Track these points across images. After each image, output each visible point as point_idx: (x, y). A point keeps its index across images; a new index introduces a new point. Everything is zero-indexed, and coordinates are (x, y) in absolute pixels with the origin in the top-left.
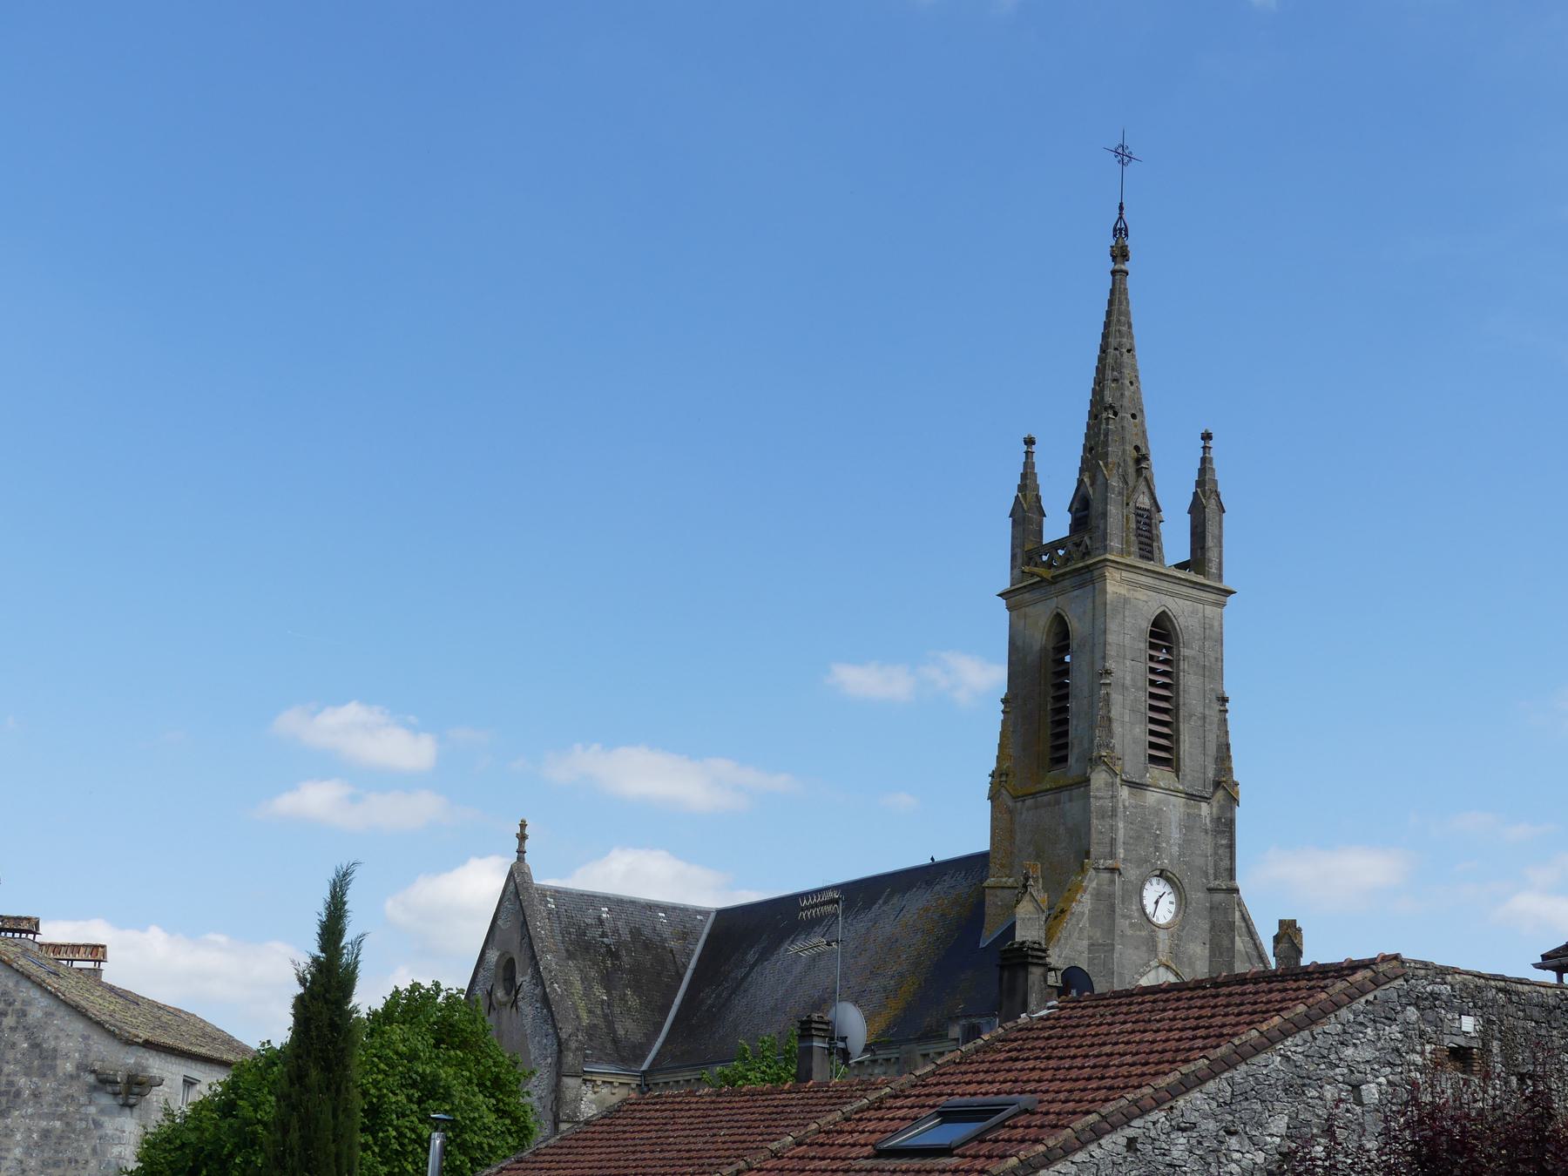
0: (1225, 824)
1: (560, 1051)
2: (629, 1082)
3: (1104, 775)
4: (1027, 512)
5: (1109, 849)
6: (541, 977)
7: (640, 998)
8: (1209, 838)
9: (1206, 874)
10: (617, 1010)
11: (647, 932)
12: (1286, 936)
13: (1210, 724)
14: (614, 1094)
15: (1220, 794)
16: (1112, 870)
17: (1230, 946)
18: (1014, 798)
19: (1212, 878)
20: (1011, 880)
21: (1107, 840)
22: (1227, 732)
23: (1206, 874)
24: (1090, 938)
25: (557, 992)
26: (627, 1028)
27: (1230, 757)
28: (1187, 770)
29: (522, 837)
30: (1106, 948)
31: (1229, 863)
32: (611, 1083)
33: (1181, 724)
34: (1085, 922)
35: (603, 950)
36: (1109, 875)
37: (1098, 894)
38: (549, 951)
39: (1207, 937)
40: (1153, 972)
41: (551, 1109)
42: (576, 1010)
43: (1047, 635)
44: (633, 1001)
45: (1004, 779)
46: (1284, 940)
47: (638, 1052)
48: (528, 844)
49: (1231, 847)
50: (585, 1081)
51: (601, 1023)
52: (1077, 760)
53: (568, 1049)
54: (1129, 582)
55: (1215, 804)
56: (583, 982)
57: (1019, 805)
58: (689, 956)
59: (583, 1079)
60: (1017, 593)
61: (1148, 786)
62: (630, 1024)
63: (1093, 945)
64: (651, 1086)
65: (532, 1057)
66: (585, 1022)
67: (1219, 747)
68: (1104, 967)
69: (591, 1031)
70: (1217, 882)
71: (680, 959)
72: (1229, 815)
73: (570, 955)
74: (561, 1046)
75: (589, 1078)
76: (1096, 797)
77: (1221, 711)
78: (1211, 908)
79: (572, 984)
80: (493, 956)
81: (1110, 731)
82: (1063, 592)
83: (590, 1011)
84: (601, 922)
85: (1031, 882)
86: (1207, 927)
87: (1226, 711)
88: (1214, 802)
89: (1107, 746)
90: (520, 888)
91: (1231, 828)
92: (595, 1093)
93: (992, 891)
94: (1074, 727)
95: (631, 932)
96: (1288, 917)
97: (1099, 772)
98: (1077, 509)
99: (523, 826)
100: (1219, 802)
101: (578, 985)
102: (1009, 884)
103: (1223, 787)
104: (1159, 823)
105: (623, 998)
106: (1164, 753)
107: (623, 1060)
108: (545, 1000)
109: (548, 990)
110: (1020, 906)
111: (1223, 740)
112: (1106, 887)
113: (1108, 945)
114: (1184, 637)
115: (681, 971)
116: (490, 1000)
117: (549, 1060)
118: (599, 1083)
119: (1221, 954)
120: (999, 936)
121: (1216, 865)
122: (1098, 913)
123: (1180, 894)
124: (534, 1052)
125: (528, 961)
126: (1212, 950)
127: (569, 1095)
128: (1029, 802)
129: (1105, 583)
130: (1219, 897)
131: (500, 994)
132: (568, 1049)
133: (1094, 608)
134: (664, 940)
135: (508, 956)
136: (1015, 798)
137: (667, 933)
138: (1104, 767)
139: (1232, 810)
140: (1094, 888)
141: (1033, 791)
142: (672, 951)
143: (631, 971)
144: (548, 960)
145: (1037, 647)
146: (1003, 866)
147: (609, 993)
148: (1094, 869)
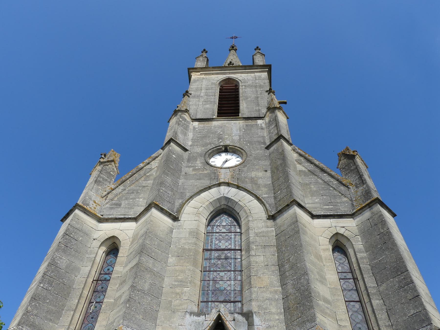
54: (205, 74)
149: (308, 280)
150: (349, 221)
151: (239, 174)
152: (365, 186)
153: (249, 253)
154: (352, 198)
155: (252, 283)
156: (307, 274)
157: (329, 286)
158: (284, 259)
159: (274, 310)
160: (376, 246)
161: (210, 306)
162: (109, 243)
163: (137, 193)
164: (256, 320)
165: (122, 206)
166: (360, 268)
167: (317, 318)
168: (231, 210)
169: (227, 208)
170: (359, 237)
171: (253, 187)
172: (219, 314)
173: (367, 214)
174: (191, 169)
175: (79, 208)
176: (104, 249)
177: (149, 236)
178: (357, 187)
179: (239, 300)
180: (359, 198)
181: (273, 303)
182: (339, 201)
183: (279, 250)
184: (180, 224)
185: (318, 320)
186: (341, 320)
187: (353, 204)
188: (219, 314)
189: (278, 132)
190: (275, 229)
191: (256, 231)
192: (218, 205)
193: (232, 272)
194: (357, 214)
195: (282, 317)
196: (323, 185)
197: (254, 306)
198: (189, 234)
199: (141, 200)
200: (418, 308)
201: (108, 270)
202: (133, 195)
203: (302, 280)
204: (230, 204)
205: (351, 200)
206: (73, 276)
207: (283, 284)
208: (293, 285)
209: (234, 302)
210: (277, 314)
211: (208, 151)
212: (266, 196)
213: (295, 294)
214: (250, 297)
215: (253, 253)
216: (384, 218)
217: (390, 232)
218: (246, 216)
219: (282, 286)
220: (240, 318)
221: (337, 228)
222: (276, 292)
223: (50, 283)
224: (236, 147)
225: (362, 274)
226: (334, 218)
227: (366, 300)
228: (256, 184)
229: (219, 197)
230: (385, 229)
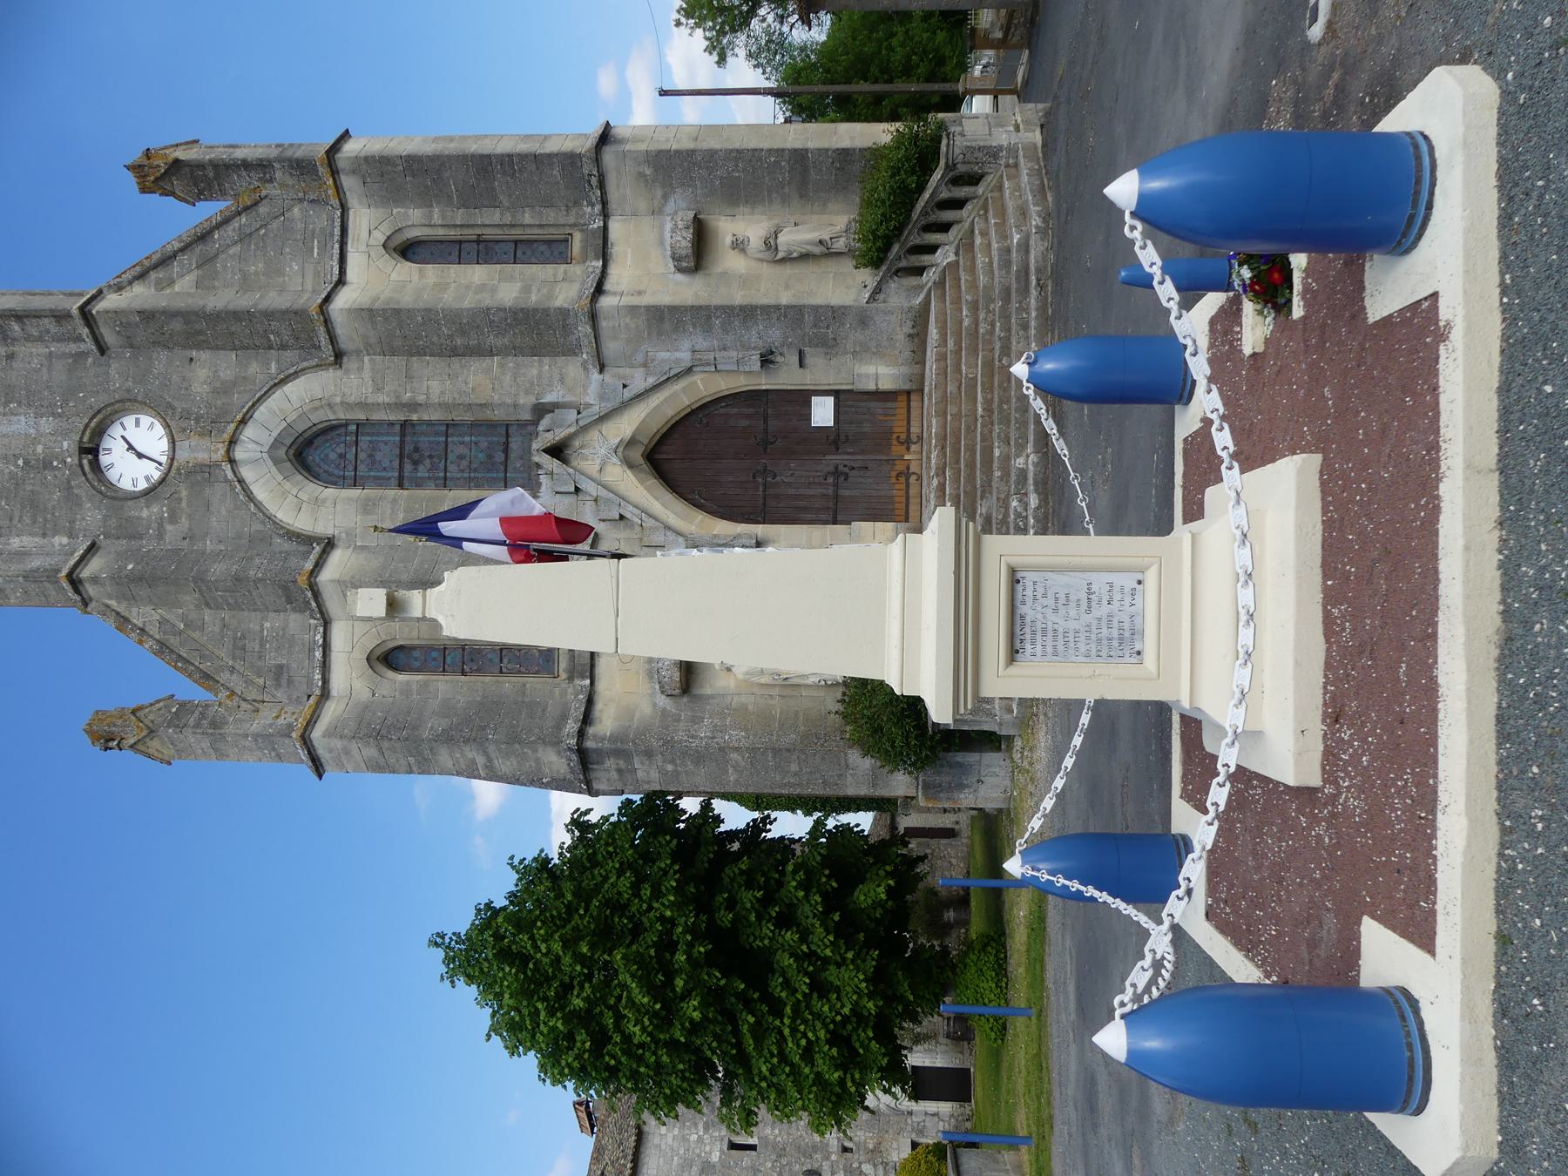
149: (499, 309)
150: (355, 217)
151: (197, 420)
152: (276, 165)
153: (420, 405)
154: (295, 196)
155: (484, 402)
156: (488, 309)
157: (495, 282)
158: (441, 345)
159: (535, 372)
160: (426, 186)
161: (513, 475)
162: (381, 668)
163: (243, 637)
164: (549, 398)
165: (284, 662)
166: (462, 226)
167: (753, 208)
168: (301, 439)
169: (294, 447)
170: (395, 211)
171: (245, 391)
172: (544, 451)
173: (347, 181)
174: (169, 528)
175: (308, 732)
176: (390, 674)
177: (391, 576)
178: (271, 181)
179: (504, 428)
180: (303, 185)
181: (522, 371)
182: (300, 226)
183: (421, 353)
184: (343, 535)
185: (566, 305)
186: (555, 275)
187: (313, 201)
188: (544, 451)
189: (55, 317)
190: (369, 354)
191: (370, 390)
192: (288, 464)
193: (449, 439)
194: (343, 201)
195: (546, 360)
196: (249, 245)
197: (527, 400)
198: (371, 514)
199: (268, 625)
200: (554, 163)
201: (435, 659)
202: (249, 647)
203: (496, 319)
204: (288, 442)
205: (301, 200)
206: (459, 706)
207: (491, 354)
208: (496, 336)
209: (508, 436)
210: (541, 366)
211: (100, 492)
212: (273, 366)
213: (514, 334)
214: (508, 406)
215: (421, 399)
216: (374, 157)
217: (409, 156)
218: (327, 408)
219: (492, 355)
220: (545, 422)
221: (371, 242)
222: (502, 366)
223: (483, 728)
224: (87, 426)
225: (472, 226)
226: (346, 243)
227: (518, 231)
228: (234, 384)
229: (270, 463)
230: (399, 162)
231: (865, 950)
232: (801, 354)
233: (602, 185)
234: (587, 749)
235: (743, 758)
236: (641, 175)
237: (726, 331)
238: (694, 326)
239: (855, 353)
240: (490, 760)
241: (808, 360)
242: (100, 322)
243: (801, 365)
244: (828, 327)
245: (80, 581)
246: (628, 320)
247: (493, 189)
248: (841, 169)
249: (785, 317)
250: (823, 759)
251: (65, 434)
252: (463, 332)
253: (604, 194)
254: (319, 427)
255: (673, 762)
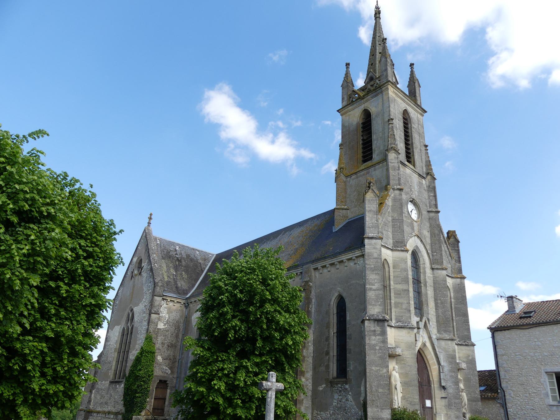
0: (432, 188)
1: (155, 287)
2: (181, 301)
3: (394, 154)
4: (347, 82)
5: (398, 182)
6: (151, 262)
7: (188, 275)
8: (426, 193)
9: (426, 206)
10: (178, 278)
11: (192, 256)
12: (453, 236)
13: (423, 153)
14: (174, 306)
15: (429, 177)
16: (401, 190)
17: (438, 233)
18: (346, 177)
19: (428, 207)
20: (346, 207)
21: (397, 178)
22: (429, 157)
23: (426, 206)
24: (392, 217)
25: (156, 267)
26: (182, 284)
27: (431, 165)
28: (418, 166)
29: (150, 218)
30: (400, 221)
31: (435, 202)
32: (174, 301)
33: (414, 149)
34: (389, 210)
35: (176, 259)
36: (399, 192)
37: (394, 199)
38: (155, 254)
39: (429, 229)
40: (413, 237)
41: (149, 309)
42: (163, 275)
43: (360, 118)
44: (185, 276)
45: (342, 170)
46: (452, 237)
47: (185, 292)
48: (152, 221)
49: (435, 196)
50: (163, 299)
51: (172, 281)
52: (377, 155)
53: (158, 286)
54: (396, 94)
55: (427, 181)
56: (167, 267)
57: (348, 179)
58: (206, 266)
59: (163, 299)
60: (346, 107)
61: (407, 165)
62: (183, 283)
63: (394, 219)
64: (189, 303)
65: (144, 291)
66: (166, 279)
67: (426, 162)
68: (399, 228)
69: (168, 283)
70: (431, 209)
71: (203, 266)
72: (433, 185)
73: (163, 258)
74: (155, 285)
75: (165, 298)
76: (391, 162)
77: (425, 150)
78: (429, 219)
79: (162, 267)
80: (135, 259)
81: (395, 139)
82: (367, 101)
83: (168, 277)
84: (176, 250)
85: (372, 184)
86: (428, 225)
87: (428, 150)
88: (427, 180)
89: (394, 144)
90: (147, 234)
91: (434, 190)
92: (167, 304)
93: (338, 210)
94: (375, 144)
95: (186, 255)
96: (452, 229)
97: (392, 153)
98: (368, 82)
99: (151, 215)
100: (428, 180)
101: (165, 267)
102: (345, 208)
103: (429, 174)
104: (411, 181)
105: (181, 274)
106: (409, 157)
107: (179, 293)
108: (151, 270)
109: (152, 266)
110: (367, 194)
111: (428, 159)
112: (398, 196)
113: (400, 219)
114: (413, 121)
115: (203, 270)
116: (132, 274)
117: (150, 291)
118: (169, 300)
119: (435, 237)
120: (344, 226)
121: (430, 203)
122: (395, 207)
123: (419, 210)
124: (145, 289)
125: (147, 257)
126: (431, 235)
127: (156, 303)
128: (353, 177)
129: (388, 91)
130: (432, 215)
131: (136, 272)
132: (158, 286)
133: (383, 101)
134: (197, 260)
135: (140, 259)
136: (347, 177)
137: (199, 258)
138: (394, 151)
139: (434, 183)
140: (392, 197)
141: (356, 172)
142: (200, 263)
143: (185, 267)
144: (154, 256)
145: (355, 123)
146: (342, 202)
147: (176, 272)
148: (393, 189)
173: (459, 280)
205: (452, 267)
231: (22, 390)
232: (446, 398)
233: (466, 345)
234: (385, 322)
235: (384, 373)
236: (469, 356)
237: (451, 376)
238: (451, 367)
239: (447, 414)
240: (374, 290)
241: (444, 400)
242: (436, 214)
243: (442, 398)
244: (455, 407)
245: (429, 191)
246: (451, 349)
247: (460, 316)
248: (476, 412)
249: (457, 394)
250: (386, 401)
251: (416, 196)
252: (442, 303)
253: (463, 345)
254: (418, 259)
255: (380, 349)
